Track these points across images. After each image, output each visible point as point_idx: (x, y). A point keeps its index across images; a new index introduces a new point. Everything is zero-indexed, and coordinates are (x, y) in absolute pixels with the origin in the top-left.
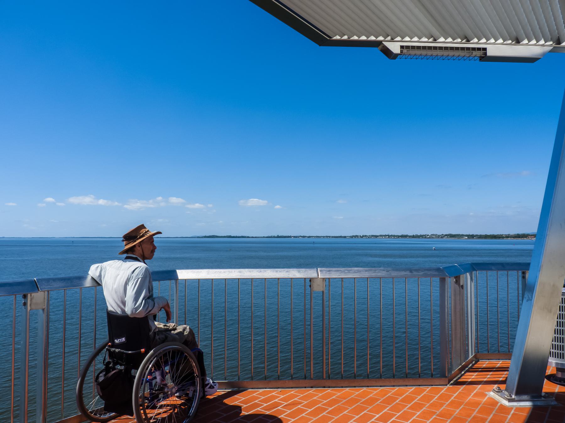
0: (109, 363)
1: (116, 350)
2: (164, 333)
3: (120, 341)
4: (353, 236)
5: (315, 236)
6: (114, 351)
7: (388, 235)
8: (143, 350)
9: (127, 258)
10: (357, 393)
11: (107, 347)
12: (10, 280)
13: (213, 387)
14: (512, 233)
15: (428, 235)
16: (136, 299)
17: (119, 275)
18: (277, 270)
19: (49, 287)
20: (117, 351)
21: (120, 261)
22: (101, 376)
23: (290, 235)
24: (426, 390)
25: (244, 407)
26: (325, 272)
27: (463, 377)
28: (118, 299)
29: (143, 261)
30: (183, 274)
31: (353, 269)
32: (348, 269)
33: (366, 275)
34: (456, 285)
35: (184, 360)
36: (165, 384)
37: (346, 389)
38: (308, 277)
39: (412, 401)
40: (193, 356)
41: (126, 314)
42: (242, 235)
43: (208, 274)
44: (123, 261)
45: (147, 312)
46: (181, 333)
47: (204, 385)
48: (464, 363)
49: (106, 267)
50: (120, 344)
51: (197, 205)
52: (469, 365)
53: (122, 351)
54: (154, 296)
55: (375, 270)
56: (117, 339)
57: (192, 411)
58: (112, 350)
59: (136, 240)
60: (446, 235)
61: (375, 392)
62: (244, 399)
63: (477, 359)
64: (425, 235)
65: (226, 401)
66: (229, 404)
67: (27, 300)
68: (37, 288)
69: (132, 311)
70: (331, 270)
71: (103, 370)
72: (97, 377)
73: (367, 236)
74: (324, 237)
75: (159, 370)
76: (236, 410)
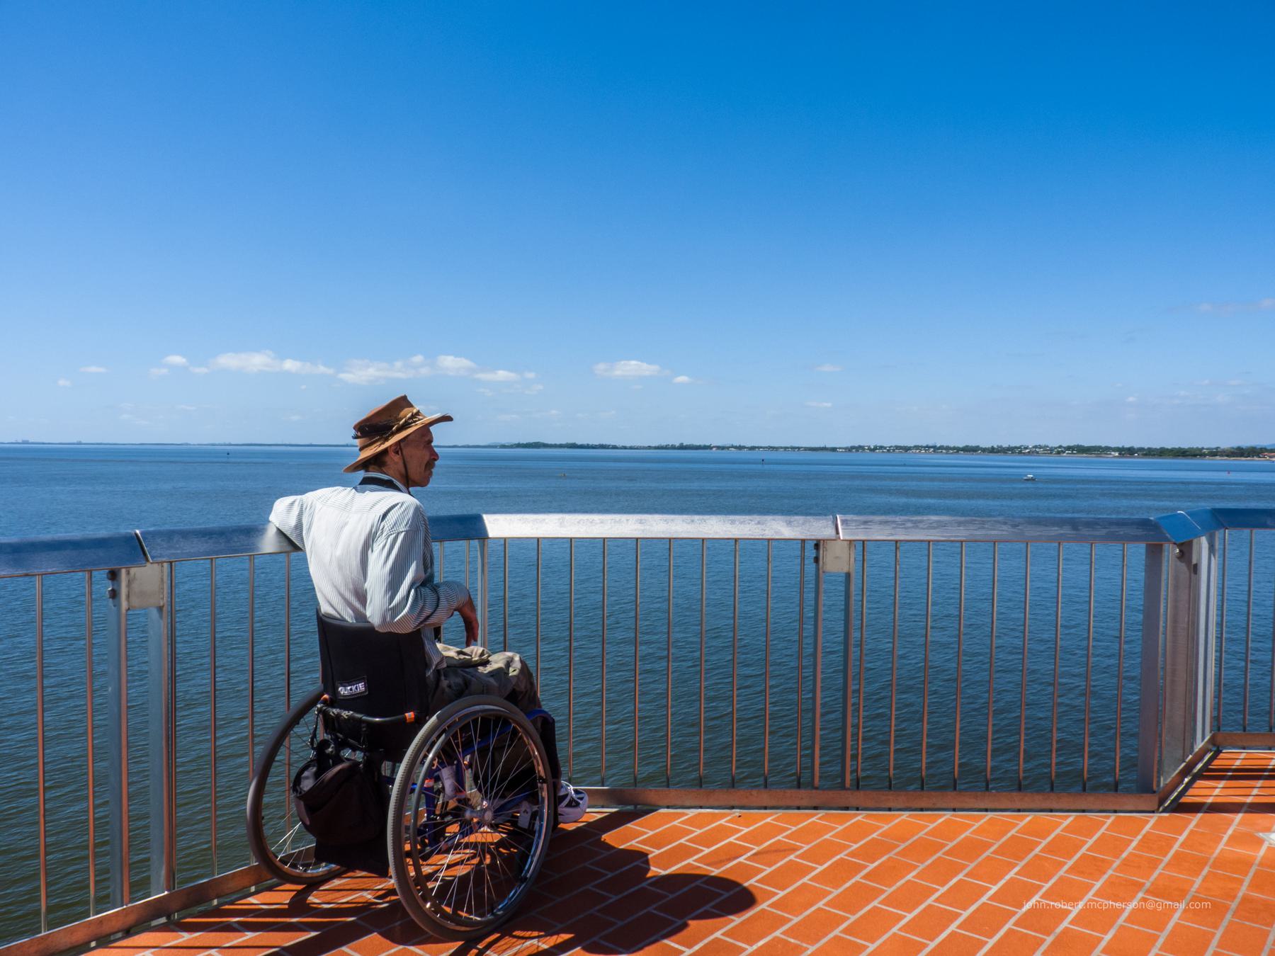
0: (324, 744)
1: (343, 714)
2: (459, 671)
3: (351, 689)
4: (853, 448)
5: (767, 446)
6: (338, 716)
7: (934, 447)
8: (410, 715)
9: (366, 481)
10: (932, 826)
11: (319, 706)
12: (76, 534)
13: (577, 805)
14: (1226, 443)
15: (1026, 448)
16: (393, 586)
17: (346, 524)
18: (732, 517)
19: (173, 551)
20: (345, 716)
21: (349, 489)
22: (307, 778)
23: (709, 444)
24: (1105, 823)
25: (653, 854)
26: (854, 524)
27: (1191, 792)
28: (346, 585)
29: (406, 491)
30: (499, 526)
31: (925, 518)
32: (913, 519)
33: (961, 533)
34: (1179, 563)
35: (512, 741)
36: (465, 799)
37: (903, 815)
38: (813, 537)
39: (1076, 852)
40: (531, 728)
41: (366, 625)
42: (601, 443)
43: (562, 525)
44: (356, 490)
45: (422, 619)
46: (500, 674)
47: (557, 799)
48: (1190, 756)
49: (314, 503)
50: (353, 699)
51: (502, 375)
52: (1197, 764)
53: (359, 716)
54: (436, 580)
55: (983, 523)
56: (345, 686)
57: (532, 865)
58: (331, 713)
59: (389, 436)
60: (1069, 448)
61: (977, 825)
62: (651, 833)
63: (1216, 747)
64: (1020, 447)
65: (607, 837)
66: (616, 846)
67: (119, 585)
68: (142, 556)
69: (384, 618)
70: (870, 521)
71: (312, 761)
72: (298, 780)
73: (885, 448)
74: (786, 448)
75: (451, 764)
76: (635, 864)
